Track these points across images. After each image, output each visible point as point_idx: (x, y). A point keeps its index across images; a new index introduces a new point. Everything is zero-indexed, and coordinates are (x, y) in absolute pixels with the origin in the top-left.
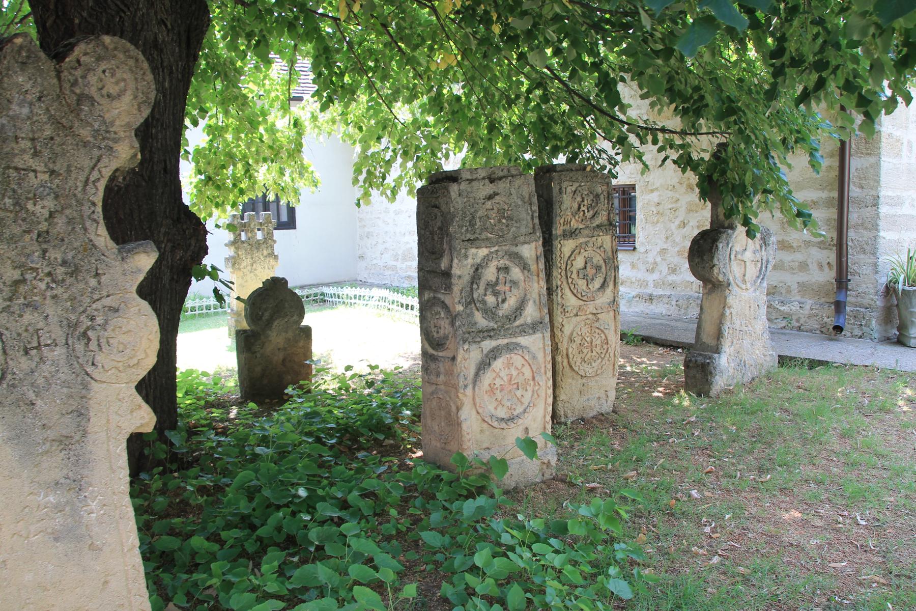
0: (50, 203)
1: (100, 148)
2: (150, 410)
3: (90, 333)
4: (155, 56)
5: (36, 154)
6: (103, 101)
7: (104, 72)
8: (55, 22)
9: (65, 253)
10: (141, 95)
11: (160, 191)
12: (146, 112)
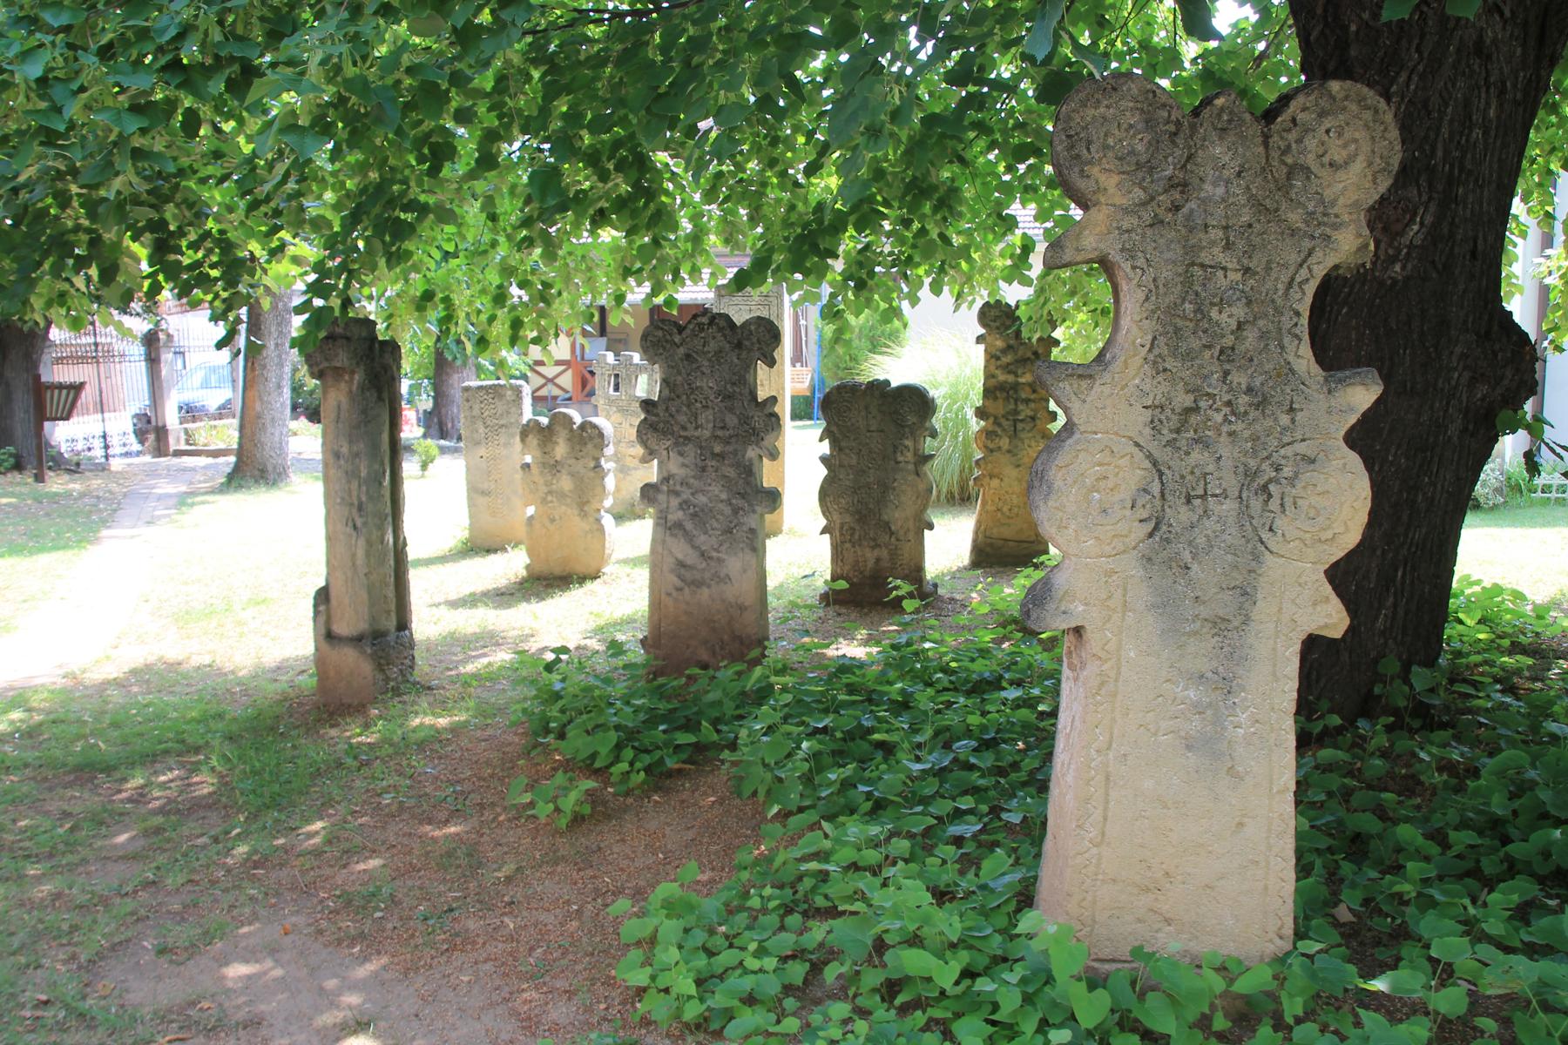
0: (1239, 311)
1: (1313, 237)
2: (1341, 606)
3: (1272, 487)
4: (1476, 67)
5: (1228, 246)
6: (1324, 173)
7: (1327, 132)
8: (1322, 32)
9: (1252, 376)
10: (1378, 160)
11: (1461, 287)
12: (1384, 184)
